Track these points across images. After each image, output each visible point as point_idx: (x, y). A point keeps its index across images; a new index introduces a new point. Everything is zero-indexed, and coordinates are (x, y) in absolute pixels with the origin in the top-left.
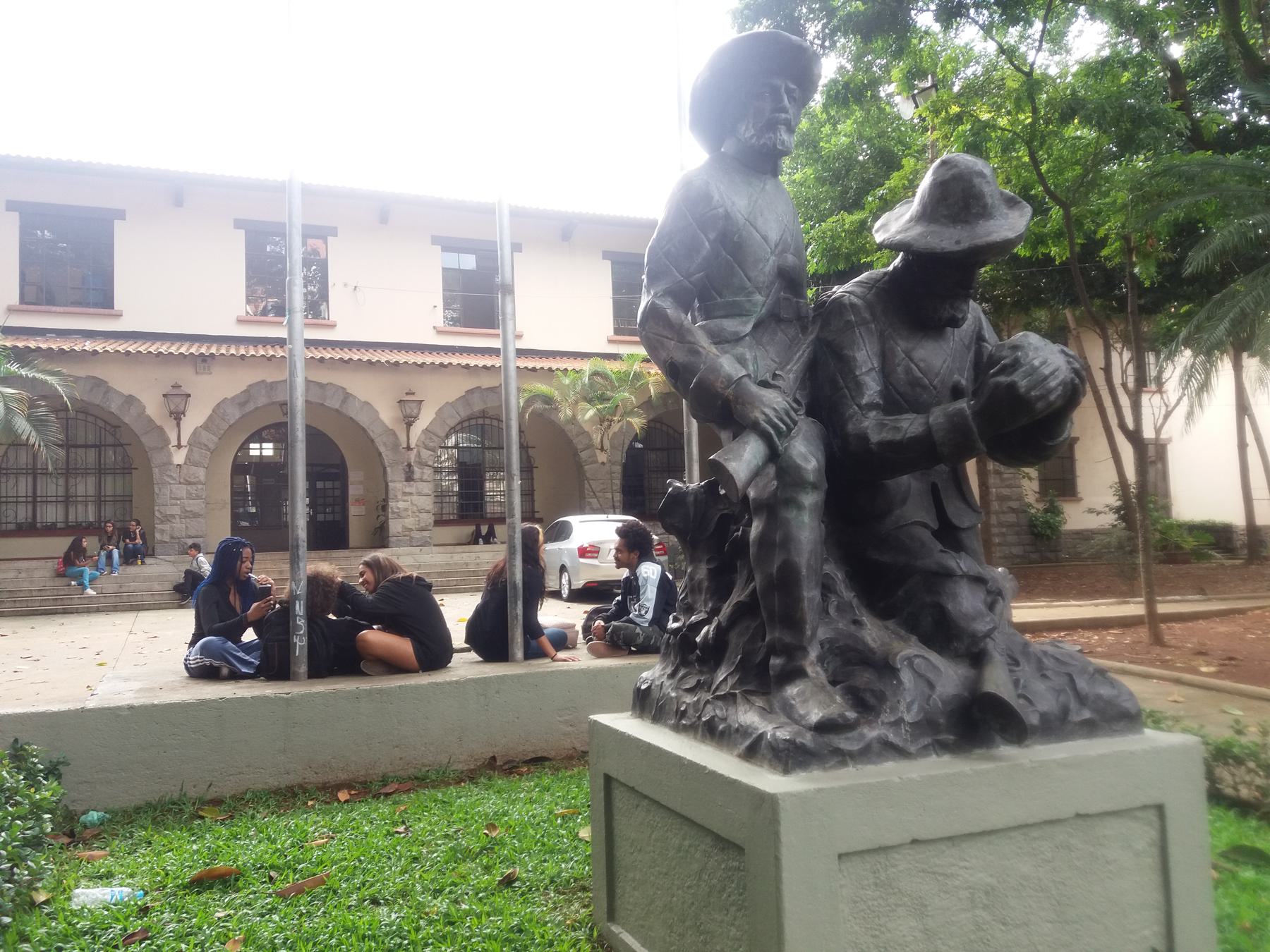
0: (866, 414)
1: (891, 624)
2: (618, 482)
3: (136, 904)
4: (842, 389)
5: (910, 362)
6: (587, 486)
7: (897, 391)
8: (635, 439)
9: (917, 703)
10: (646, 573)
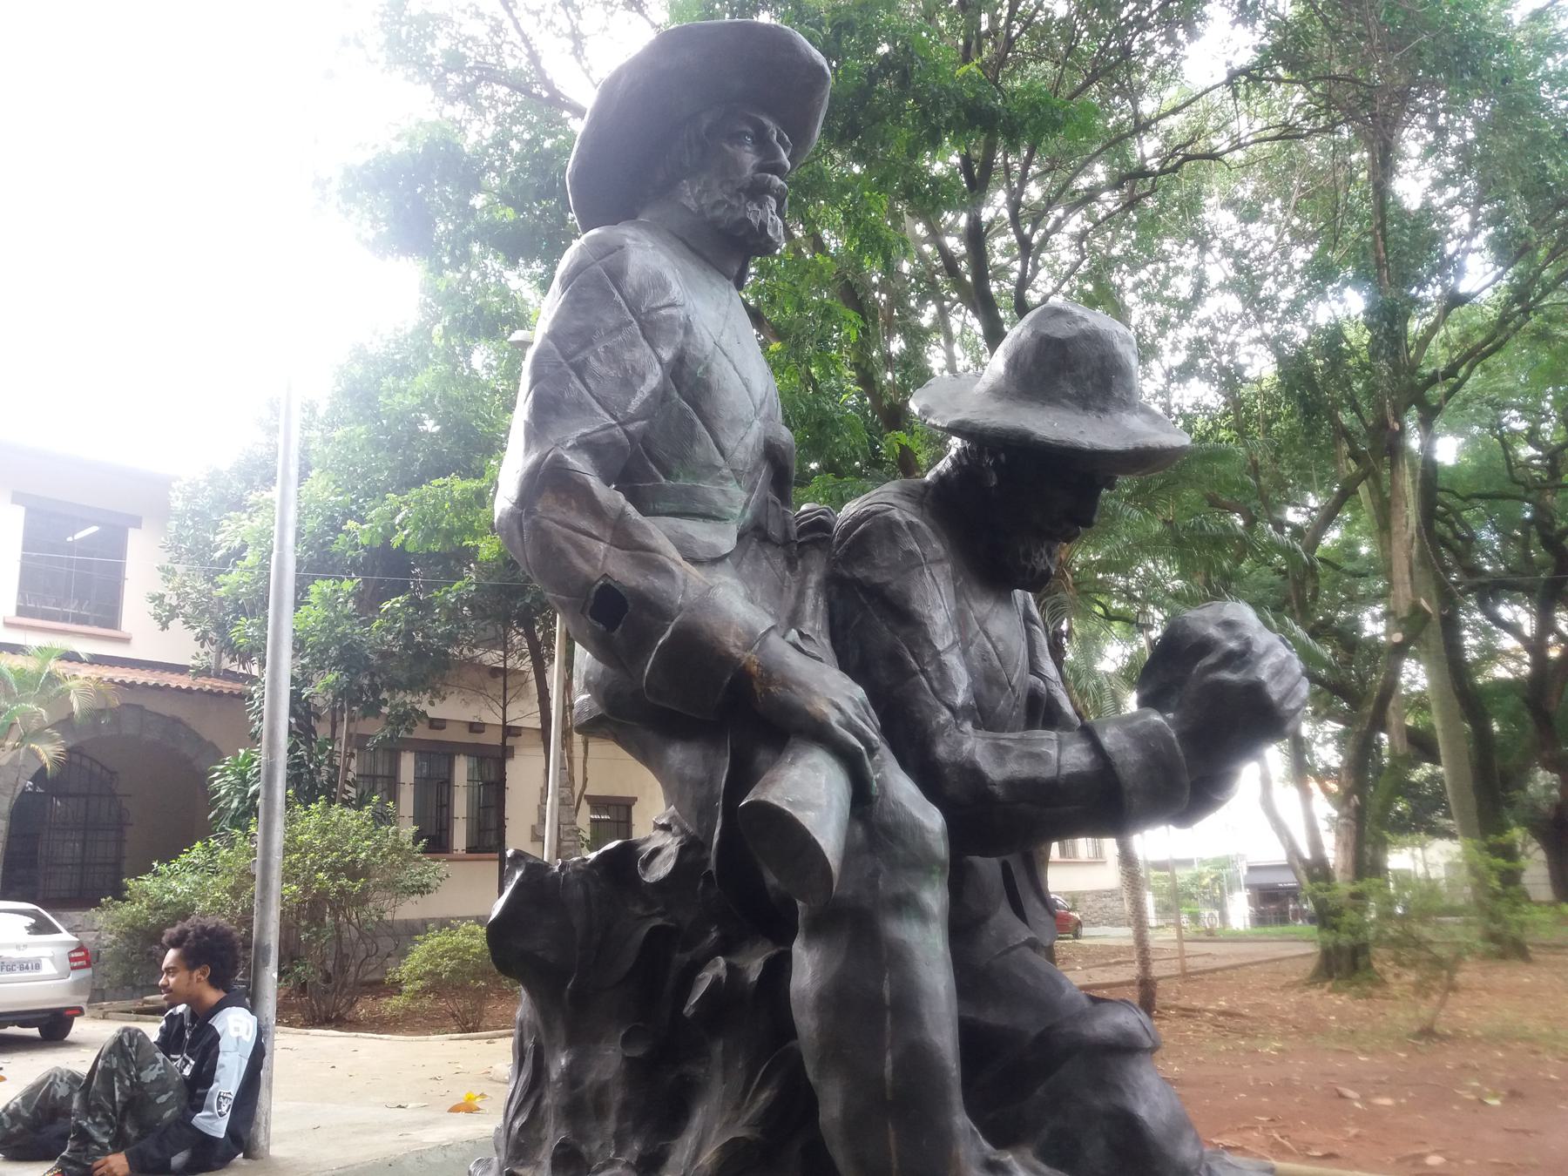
4: (914, 673)
10: (237, 1029)
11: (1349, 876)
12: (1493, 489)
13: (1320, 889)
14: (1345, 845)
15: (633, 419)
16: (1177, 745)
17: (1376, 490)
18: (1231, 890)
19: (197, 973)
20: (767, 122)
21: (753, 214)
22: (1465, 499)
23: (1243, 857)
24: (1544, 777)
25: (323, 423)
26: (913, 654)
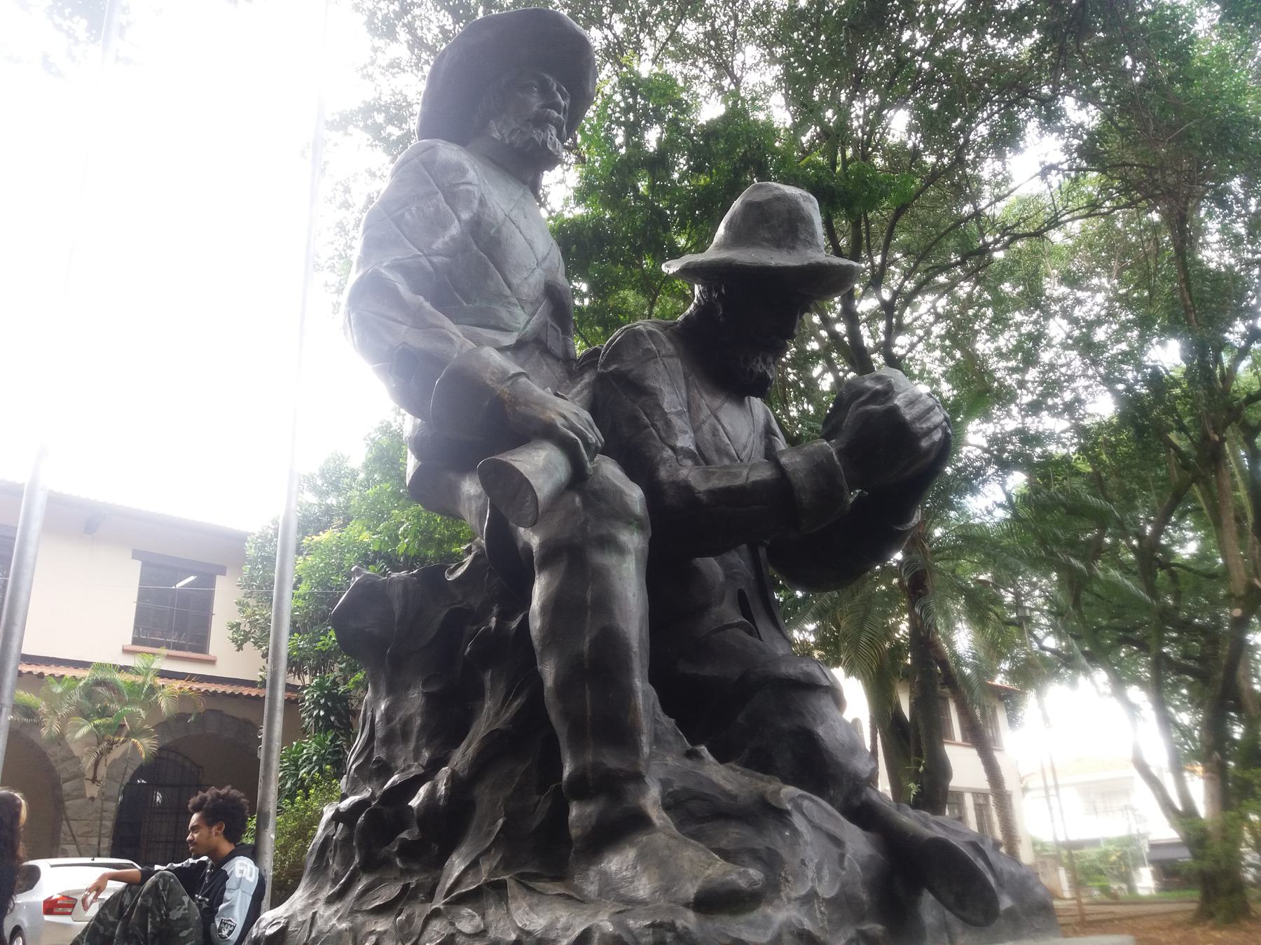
1: (732, 764)
2: (109, 824)
6: (65, 828)
8: (140, 772)
9: (826, 867)
15: (437, 254)
16: (836, 458)
19: (214, 829)
20: (547, 77)
21: (537, 135)
23: (1144, 836)
25: (361, 485)
26: (646, 414)
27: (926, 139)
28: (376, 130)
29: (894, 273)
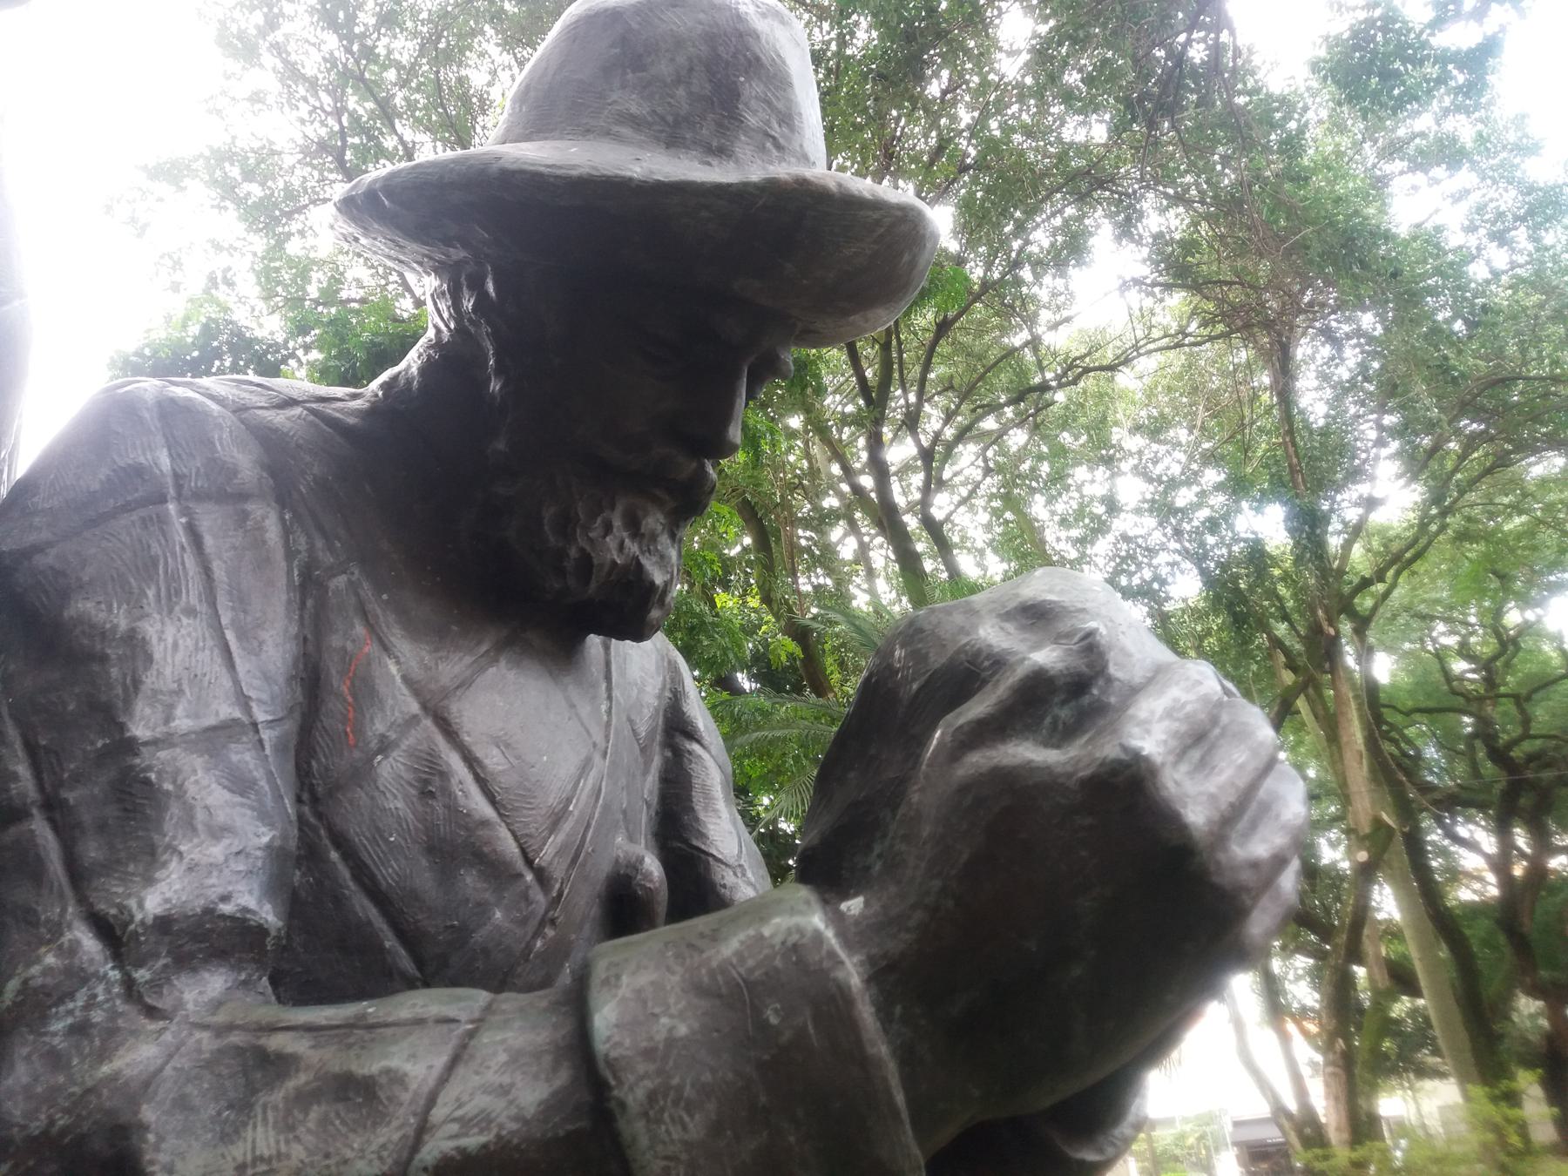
0: (156, 985)
3: (725, 650)
5: (440, 740)
7: (361, 872)
11: (1346, 1136)
12: (1431, 704)
13: (1317, 1158)
14: (1336, 1099)
16: (866, 1012)
17: (1317, 703)
18: (1217, 1149)
22: (1408, 714)
24: (1527, 1005)
26: (32, 750)
27: (971, 244)
28: (228, 190)
29: (929, 416)
